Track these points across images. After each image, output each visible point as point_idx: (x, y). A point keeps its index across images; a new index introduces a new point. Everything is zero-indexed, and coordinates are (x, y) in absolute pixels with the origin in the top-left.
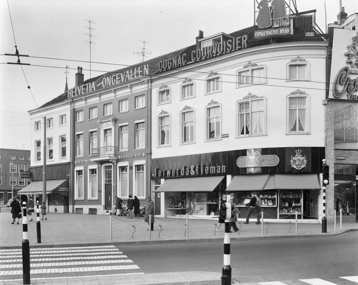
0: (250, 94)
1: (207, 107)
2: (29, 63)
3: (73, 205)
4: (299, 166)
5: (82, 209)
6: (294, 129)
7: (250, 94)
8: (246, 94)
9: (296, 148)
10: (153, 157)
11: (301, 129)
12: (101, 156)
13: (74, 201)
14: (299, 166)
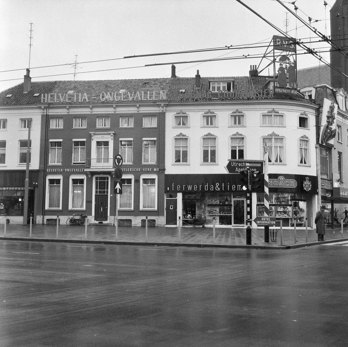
0: (273, 133)
1: (203, 137)
2: (250, 67)
3: (43, 215)
4: (307, 189)
5: (130, 221)
6: (178, 161)
7: (273, 133)
8: (270, 133)
9: (306, 176)
10: (167, 172)
11: (281, 161)
12: (91, 168)
13: (44, 211)
14: (307, 189)
